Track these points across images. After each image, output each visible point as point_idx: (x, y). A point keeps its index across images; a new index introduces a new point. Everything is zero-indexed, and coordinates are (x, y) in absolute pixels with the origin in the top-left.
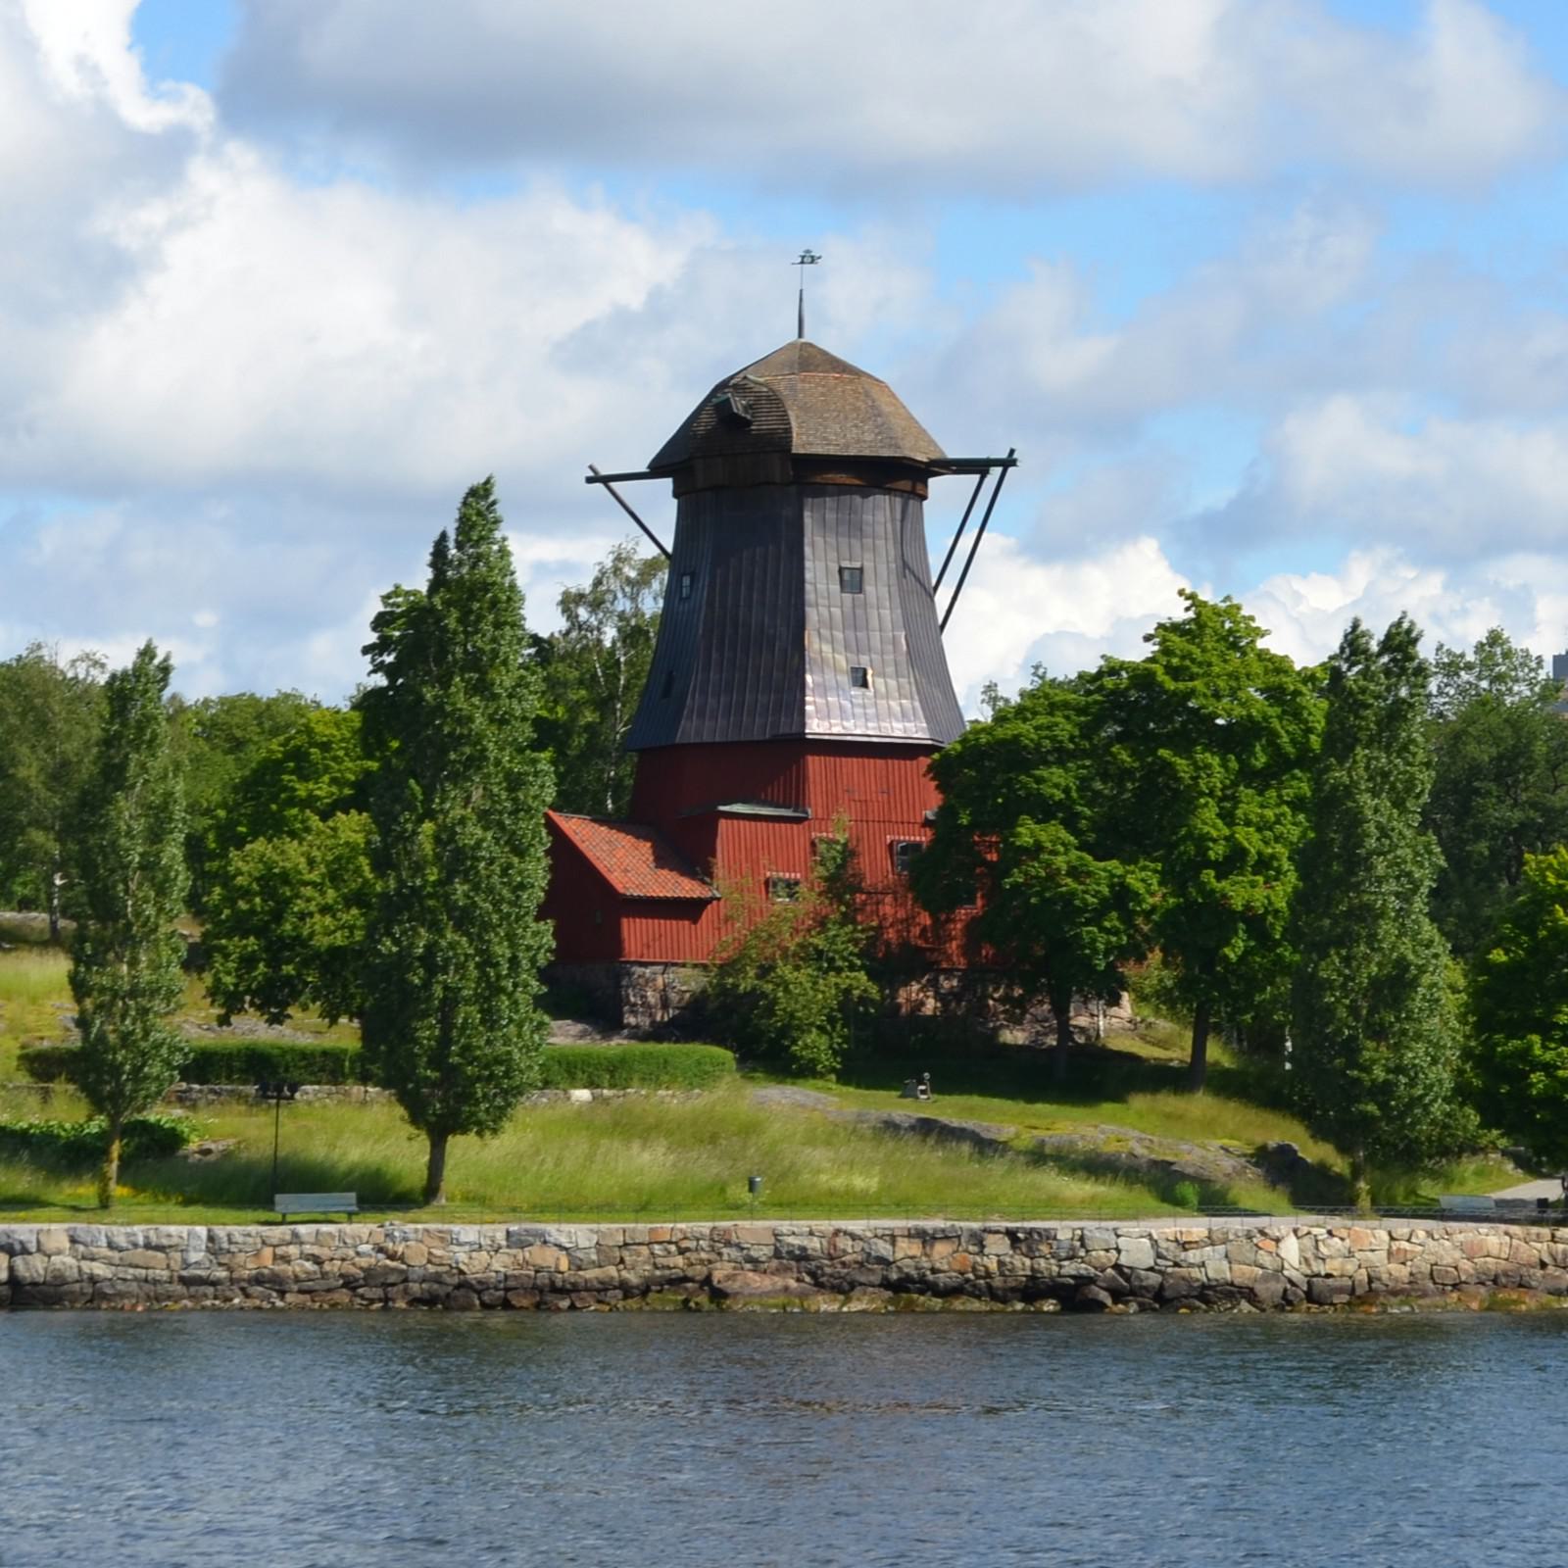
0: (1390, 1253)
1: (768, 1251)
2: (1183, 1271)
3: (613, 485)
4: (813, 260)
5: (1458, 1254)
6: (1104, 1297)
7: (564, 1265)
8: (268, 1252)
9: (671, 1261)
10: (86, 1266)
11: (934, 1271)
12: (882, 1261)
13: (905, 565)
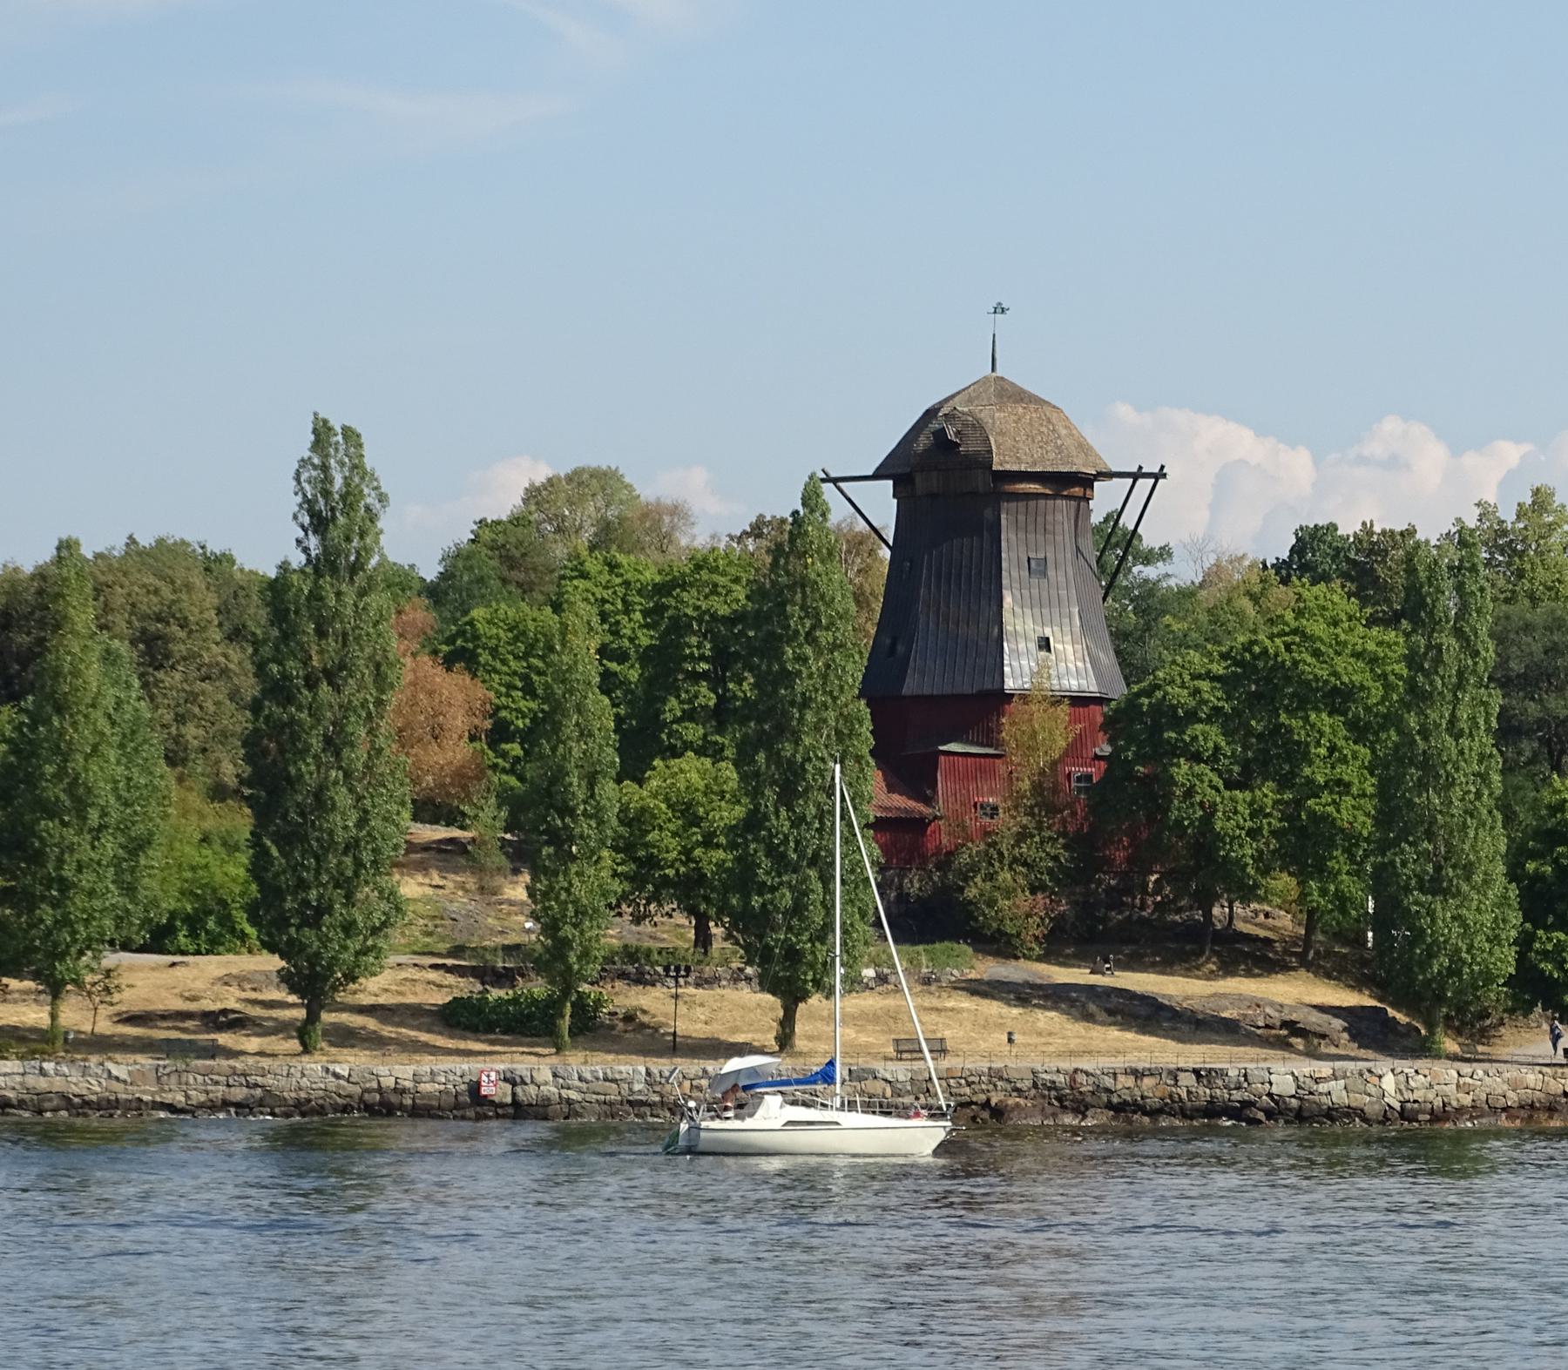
0: (1458, 1086)
1: (1029, 1083)
2: (1316, 1098)
3: (841, 485)
4: (1003, 311)
5: (1505, 1087)
6: (1261, 1116)
7: (889, 1092)
8: (687, 1084)
9: (962, 1091)
10: (564, 1093)
11: (1143, 1097)
12: (1108, 1090)
13: (1078, 549)
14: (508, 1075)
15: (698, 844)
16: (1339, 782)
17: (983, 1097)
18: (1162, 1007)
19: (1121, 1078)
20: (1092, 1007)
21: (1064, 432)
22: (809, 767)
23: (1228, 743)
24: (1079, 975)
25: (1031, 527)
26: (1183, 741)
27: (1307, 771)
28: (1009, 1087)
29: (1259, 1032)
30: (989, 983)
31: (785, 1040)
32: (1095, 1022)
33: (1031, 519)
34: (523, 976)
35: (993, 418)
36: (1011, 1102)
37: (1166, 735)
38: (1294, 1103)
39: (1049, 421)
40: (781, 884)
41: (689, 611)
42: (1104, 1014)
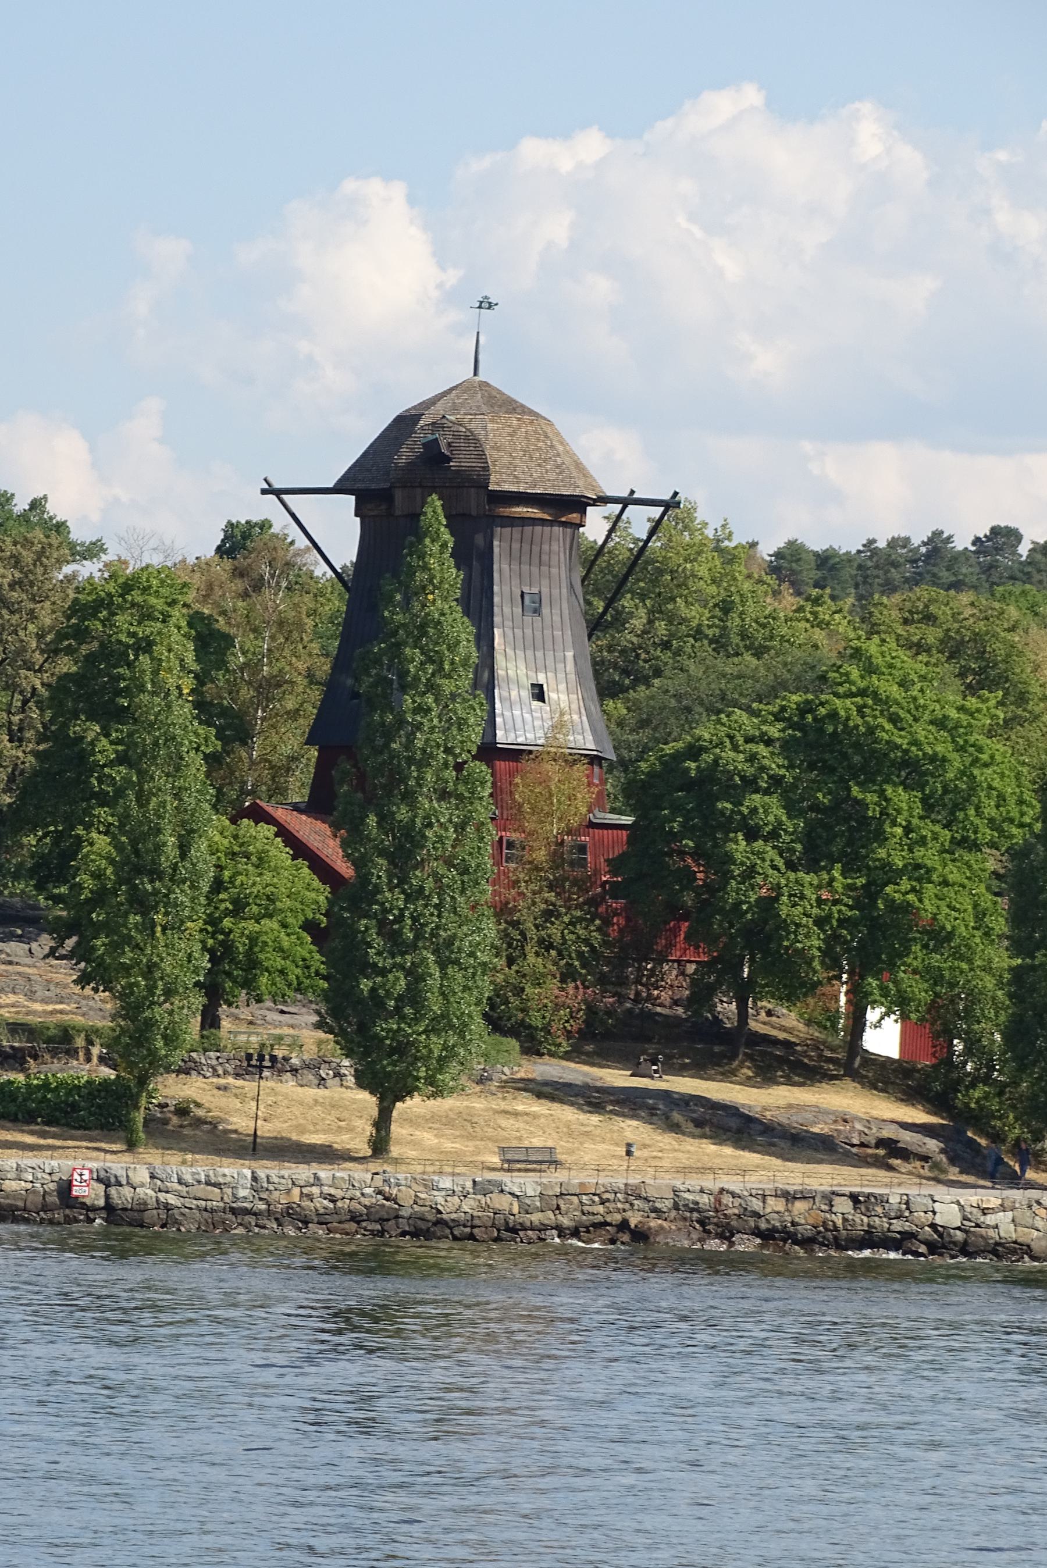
1: (669, 1203)
2: (982, 1231)
3: (284, 497)
4: (490, 306)
6: (923, 1249)
7: (516, 1210)
8: (296, 1191)
10: (162, 1196)
11: (793, 1224)
12: (757, 1215)
14: (102, 1174)
15: (227, 913)
16: (918, 867)
17: (618, 1217)
18: (749, 1120)
19: (771, 1201)
20: (677, 1117)
21: (561, 448)
22: (429, 833)
23: (789, 817)
24: (617, 1078)
25: (525, 558)
26: (740, 813)
27: (882, 853)
28: (646, 1206)
29: (854, 1150)
30: (546, 1083)
31: (380, 1145)
32: (684, 1134)
33: (526, 547)
34: (35, 1057)
35: (485, 428)
36: (653, 1224)
37: (719, 805)
38: (959, 1236)
39: (547, 437)
40: (395, 965)
41: (123, 638)
42: (691, 1125)
